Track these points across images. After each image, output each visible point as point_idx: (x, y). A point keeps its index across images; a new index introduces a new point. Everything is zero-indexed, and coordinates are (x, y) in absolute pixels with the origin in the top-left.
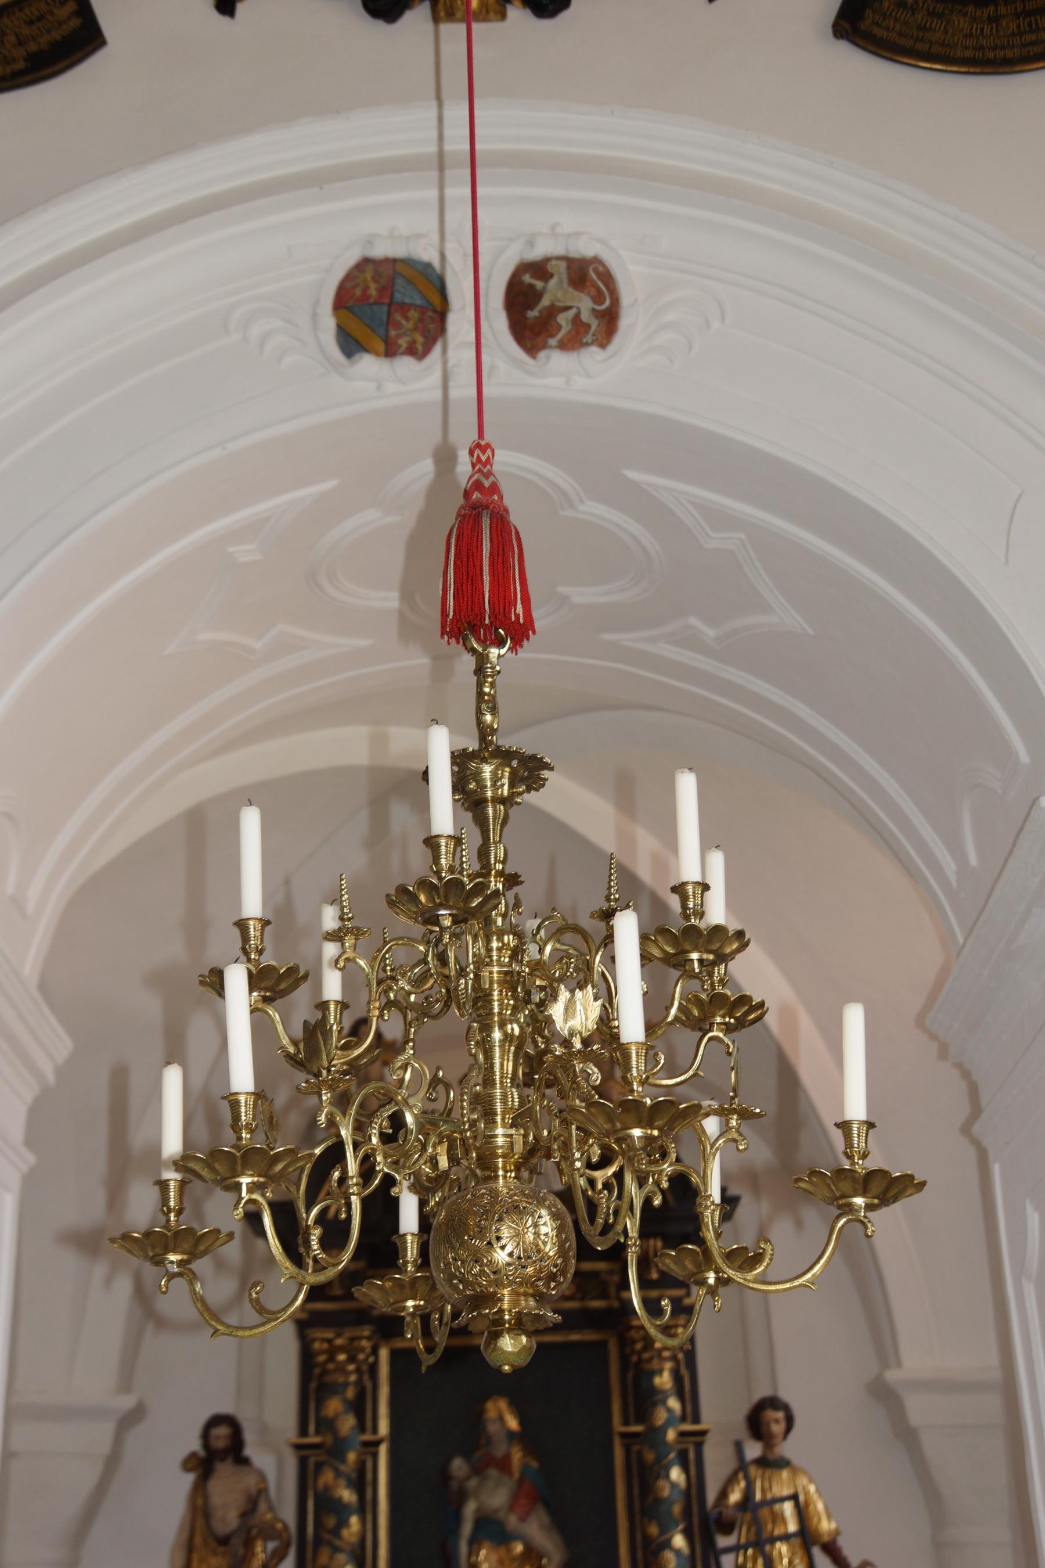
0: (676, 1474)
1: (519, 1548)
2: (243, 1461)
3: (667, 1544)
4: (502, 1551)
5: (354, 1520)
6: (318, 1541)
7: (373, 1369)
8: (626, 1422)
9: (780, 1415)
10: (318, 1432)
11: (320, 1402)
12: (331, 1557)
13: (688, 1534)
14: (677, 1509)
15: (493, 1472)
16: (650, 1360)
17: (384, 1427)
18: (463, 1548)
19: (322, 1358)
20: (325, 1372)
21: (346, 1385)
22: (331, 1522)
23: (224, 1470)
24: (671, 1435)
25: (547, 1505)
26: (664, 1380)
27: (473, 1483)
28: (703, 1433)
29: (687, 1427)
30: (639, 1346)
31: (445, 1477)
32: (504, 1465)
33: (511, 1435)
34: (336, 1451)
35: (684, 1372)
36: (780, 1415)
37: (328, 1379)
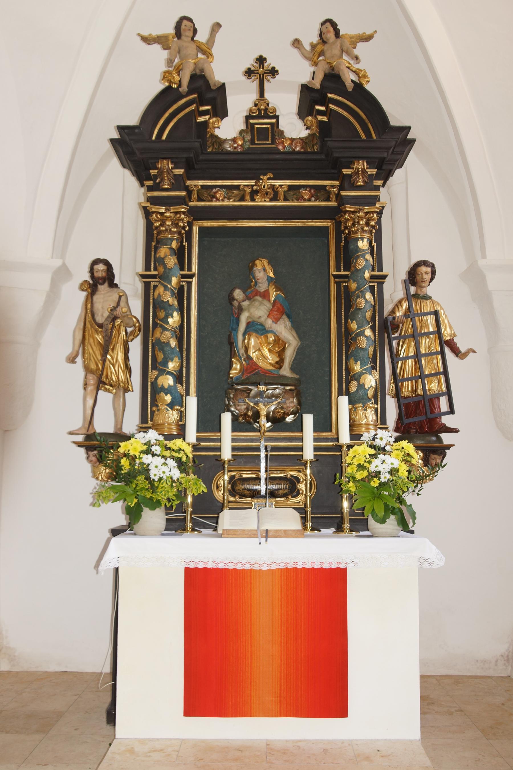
0: (368, 296)
1: (271, 338)
2: (113, 285)
3: (362, 333)
4: (263, 338)
5: (175, 314)
6: (155, 325)
7: (189, 234)
8: (338, 269)
9: (429, 269)
11: (156, 248)
12: (162, 333)
13: (373, 328)
14: (368, 315)
15: (258, 298)
16: (356, 232)
17: (195, 268)
18: (240, 337)
19: (157, 224)
20: (160, 232)
21: (172, 240)
22: (162, 314)
23: (103, 288)
24: (367, 275)
25: (289, 317)
26: (363, 244)
27: (245, 304)
28: (385, 277)
29: (375, 273)
30: (349, 224)
31: (231, 299)
32: (265, 295)
33: (270, 279)
34: (165, 277)
35: (374, 244)
36: (429, 269)
37: (161, 236)
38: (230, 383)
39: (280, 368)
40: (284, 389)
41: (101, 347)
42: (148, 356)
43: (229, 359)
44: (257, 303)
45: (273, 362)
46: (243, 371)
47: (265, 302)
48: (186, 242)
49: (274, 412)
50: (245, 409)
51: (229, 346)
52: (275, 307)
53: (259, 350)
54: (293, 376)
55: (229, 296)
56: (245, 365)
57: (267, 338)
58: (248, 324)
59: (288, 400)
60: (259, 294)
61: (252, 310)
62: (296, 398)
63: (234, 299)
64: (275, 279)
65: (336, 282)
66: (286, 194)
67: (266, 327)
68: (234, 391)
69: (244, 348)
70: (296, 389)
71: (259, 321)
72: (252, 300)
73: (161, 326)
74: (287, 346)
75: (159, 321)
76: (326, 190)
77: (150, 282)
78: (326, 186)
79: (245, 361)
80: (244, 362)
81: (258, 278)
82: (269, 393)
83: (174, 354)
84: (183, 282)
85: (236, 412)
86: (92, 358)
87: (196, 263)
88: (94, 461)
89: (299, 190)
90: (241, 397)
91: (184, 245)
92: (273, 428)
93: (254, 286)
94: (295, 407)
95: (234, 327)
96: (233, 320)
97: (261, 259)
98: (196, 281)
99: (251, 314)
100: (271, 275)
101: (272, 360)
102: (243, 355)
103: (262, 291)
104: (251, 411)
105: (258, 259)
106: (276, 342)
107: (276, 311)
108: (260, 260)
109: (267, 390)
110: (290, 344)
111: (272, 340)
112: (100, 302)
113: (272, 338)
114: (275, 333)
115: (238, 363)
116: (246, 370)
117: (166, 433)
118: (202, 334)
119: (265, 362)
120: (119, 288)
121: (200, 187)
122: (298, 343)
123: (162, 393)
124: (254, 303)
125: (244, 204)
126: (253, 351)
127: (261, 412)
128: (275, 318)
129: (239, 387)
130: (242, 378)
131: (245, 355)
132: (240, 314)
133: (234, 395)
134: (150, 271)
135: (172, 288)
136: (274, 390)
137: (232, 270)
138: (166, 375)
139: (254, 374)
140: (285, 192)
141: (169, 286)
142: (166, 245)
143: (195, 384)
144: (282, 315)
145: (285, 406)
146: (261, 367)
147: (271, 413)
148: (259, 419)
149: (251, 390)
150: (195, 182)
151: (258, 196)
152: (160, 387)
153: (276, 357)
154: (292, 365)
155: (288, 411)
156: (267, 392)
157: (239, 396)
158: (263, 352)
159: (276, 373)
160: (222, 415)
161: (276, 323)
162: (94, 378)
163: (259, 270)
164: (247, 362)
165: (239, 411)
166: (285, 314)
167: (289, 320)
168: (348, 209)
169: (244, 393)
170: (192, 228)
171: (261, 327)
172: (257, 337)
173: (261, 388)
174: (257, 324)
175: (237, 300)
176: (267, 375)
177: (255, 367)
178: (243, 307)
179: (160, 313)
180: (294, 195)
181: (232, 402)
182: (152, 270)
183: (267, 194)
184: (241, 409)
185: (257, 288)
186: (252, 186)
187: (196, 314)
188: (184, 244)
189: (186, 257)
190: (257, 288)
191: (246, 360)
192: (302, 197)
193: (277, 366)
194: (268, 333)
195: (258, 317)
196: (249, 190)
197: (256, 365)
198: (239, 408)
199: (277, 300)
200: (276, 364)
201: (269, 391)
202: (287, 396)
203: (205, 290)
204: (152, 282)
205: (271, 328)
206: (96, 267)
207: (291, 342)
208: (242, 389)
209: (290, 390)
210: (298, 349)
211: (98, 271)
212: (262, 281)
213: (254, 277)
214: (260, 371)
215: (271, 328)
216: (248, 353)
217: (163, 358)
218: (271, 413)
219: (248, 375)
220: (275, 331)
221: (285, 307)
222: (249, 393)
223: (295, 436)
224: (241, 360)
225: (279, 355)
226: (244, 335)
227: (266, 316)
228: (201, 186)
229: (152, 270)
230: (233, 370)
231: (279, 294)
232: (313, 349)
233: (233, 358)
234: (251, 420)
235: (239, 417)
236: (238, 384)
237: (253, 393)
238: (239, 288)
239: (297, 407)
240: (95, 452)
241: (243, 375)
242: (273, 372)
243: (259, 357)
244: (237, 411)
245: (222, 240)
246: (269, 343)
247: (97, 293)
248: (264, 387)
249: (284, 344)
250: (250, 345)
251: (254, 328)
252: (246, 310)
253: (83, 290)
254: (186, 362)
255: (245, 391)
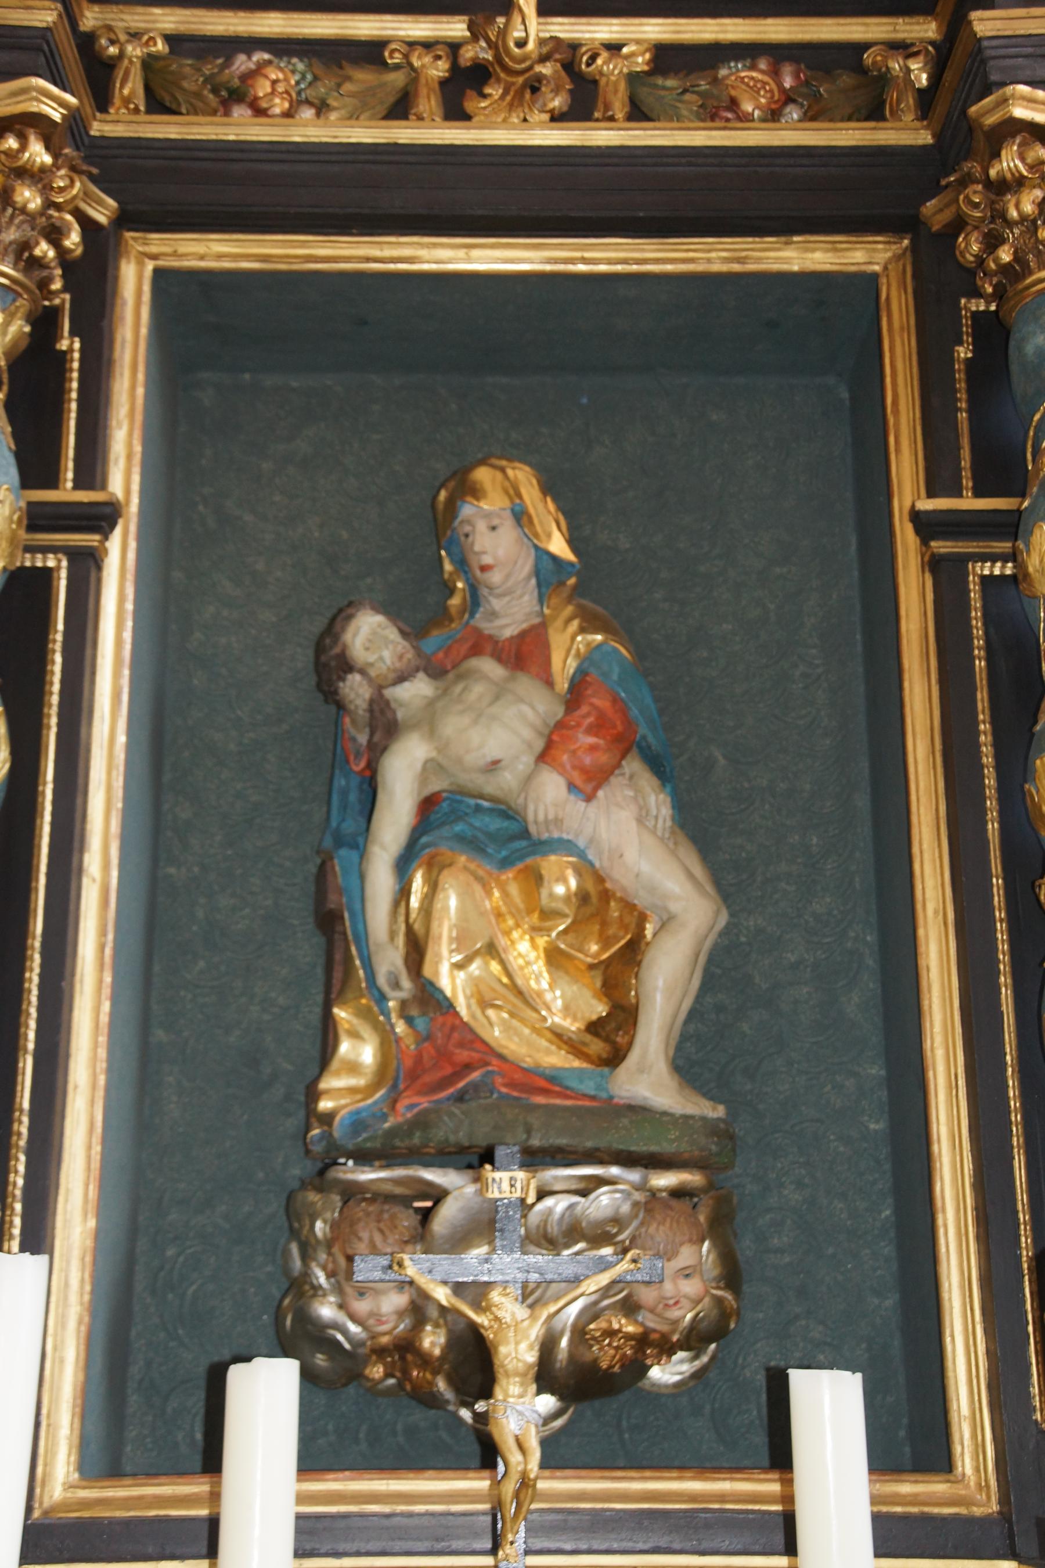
15: (489, 667)
38: (317, 1149)
39: (615, 1058)
40: (641, 1187)
43: (318, 1010)
44: (478, 690)
45: (572, 1026)
46: (396, 1079)
47: (526, 685)
48: (73, 333)
49: (579, 1332)
50: (400, 1314)
51: (320, 940)
52: (584, 709)
53: (491, 950)
54: (691, 1109)
55: (320, 648)
56: (410, 1044)
57: (535, 879)
58: (428, 805)
59: (669, 1255)
60: (489, 648)
61: (452, 725)
62: (714, 1244)
63: (346, 666)
64: (578, 574)
65: (935, 565)
66: (643, 92)
67: (530, 817)
68: (336, 1199)
69: (401, 940)
70: (711, 1186)
71: (490, 787)
72: (451, 676)
74: (649, 930)
76: (861, 69)
78: (862, 47)
79: (409, 1021)
80: (400, 1028)
81: (487, 560)
82: (550, 1211)
84: (45, 550)
85: (345, 1332)
87: (129, 457)
89: (714, 67)
90: (378, 1238)
91: (64, 353)
92: (570, 1422)
93: (462, 612)
94: (707, 1300)
95: (349, 826)
96: (344, 793)
97: (504, 463)
98: (131, 555)
99: (443, 748)
100: (558, 546)
101: (567, 1010)
102: (396, 985)
103: (508, 633)
104: (437, 1325)
105: (483, 462)
106: (588, 910)
107: (590, 730)
108: (494, 467)
109: (542, 1195)
110: (666, 923)
111: (567, 899)
113: (564, 880)
114: (582, 855)
115: (366, 1031)
116: (413, 1075)
118: (172, 870)
119: (523, 1021)
121: (160, 46)
122: (717, 912)
124: (458, 688)
125: (404, 134)
126: (457, 958)
127: (503, 1350)
128: (584, 771)
129: (367, 1175)
130: (384, 1117)
131: (406, 983)
132: (385, 749)
133: (335, 1225)
136: (584, 1193)
137: (345, 535)
139: (460, 1098)
140: (633, 78)
143: (96, 1164)
144: (623, 757)
145: (647, 1296)
146: (501, 1057)
147: (564, 1342)
148: (487, 1393)
149: (439, 1195)
150: (135, 18)
151: (485, 96)
153: (588, 994)
154: (679, 1048)
155: (664, 1328)
156: (539, 1207)
157: (365, 1235)
158: (515, 963)
159: (588, 1087)
160: (236, 1374)
161: (589, 798)
163: (488, 515)
164: (421, 1023)
165: (365, 1328)
166: (635, 749)
167: (663, 785)
168: (1020, 112)
169: (397, 1209)
170: (117, 268)
171: (506, 824)
172: (478, 879)
173: (506, 1186)
174: (478, 809)
175: (362, 672)
176: (540, 1100)
177: (463, 1055)
178: (400, 715)
180: (685, 91)
181: (324, 1268)
183: (534, 86)
184: (375, 1315)
185: (479, 621)
186: (454, 47)
187: (122, 739)
188: (64, 345)
189: (73, 415)
190: (479, 621)
191: (414, 1012)
192: (733, 104)
193: (597, 1047)
194: (545, 854)
195: (482, 763)
196: (439, 69)
197: (472, 1039)
198: (361, 1306)
199: (592, 670)
200: (588, 1038)
201: (549, 1202)
202: (660, 1232)
203: (198, 635)
205: (558, 822)
207: (674, 907)
208: (388, 1188)
209: (678, 1193)
210: (711, 960)
212: (508, 576)
213: (462, 564)
214: (499, 1080)
215: (558, 822)
216: (427, 971)
218: (564, 1342)
219: (424, 1103)
220: (581, 843)
221: (634, 712)
222: (426, 1215)
223: (722, 1498)
224: (387, 1014)
225: (605, 984)
226: (403, 866)
227: (526, 761)
228: (172, 39)
230: (338, 1074)
231: (599, 646)
232: (792, 958)
233: (343, 1004)
234: (441, 1384)
235: (366, 1361)
236: (364, 1157)
237: (448, 1214)
238: (381, 608)
239: (719, 1301)
241: (393, 1102)
242: (573, 1084)
243: (488, 995)
244: (353, 1328)
245: (295, 384)
246: (548, 915)
248: (521, 1175)
249: (631, 920)
250: (435, 925)
251: (459, 828)
252: (414, 725)
254: (39, 1021)
255: (406, 1201)
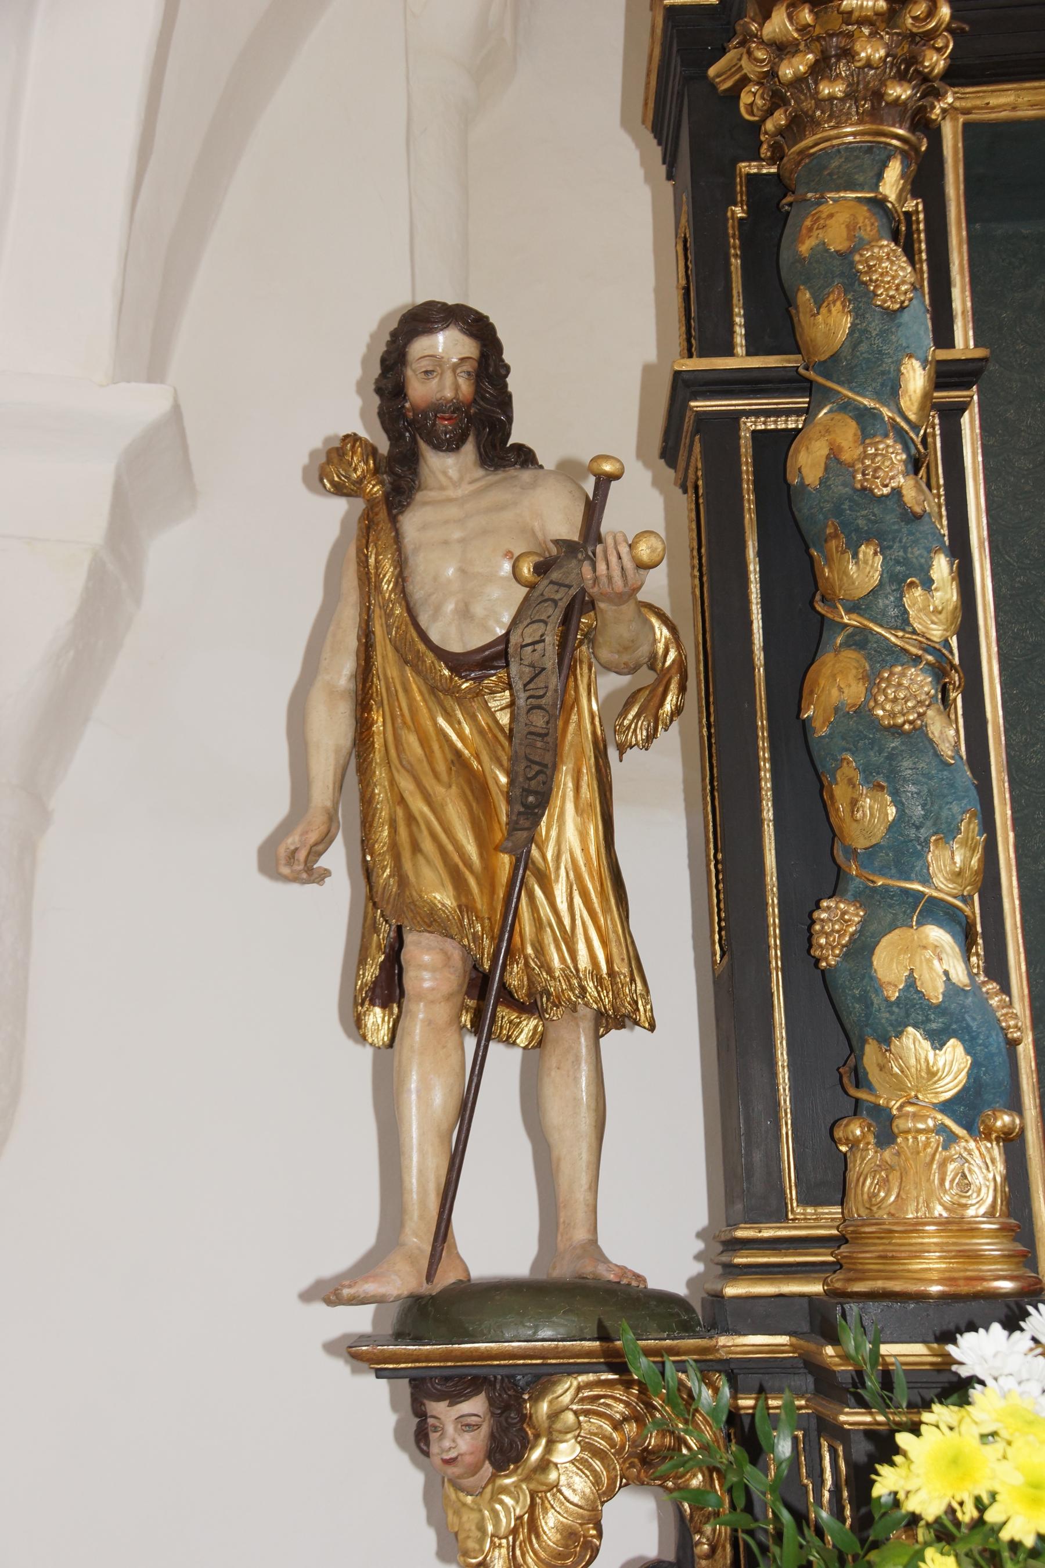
10: (752, 351)
12: (872, 680)
17: (941, 482)
41: (469, 783)
42: (759, 822)
73: (860, 640)
75: (848, 611)
77: (734, 418)
83: (959, 799)
86: (427, 845)
88: (468, 1459)
112: (446, 542)
117: (935, 1289)
120: (541, 467)
123: (910, 1029)
134: (729, 351)
135: (903, 424)
138: (920, 924)
141: (886, 413)
142: (851, 186)
152: (894, 995)
162: (448, 958)
179: (852, 568)
182: (740, 350)
204: (748, 414)
206: (420, 347)
211: (434, 368)
217: (892, 827)
229: (740, 350)
240: (475, 1406)
245: (1025, 232)
247: (419, 496)
253: (339, 490)
